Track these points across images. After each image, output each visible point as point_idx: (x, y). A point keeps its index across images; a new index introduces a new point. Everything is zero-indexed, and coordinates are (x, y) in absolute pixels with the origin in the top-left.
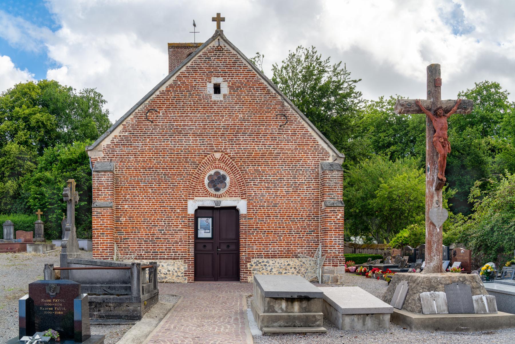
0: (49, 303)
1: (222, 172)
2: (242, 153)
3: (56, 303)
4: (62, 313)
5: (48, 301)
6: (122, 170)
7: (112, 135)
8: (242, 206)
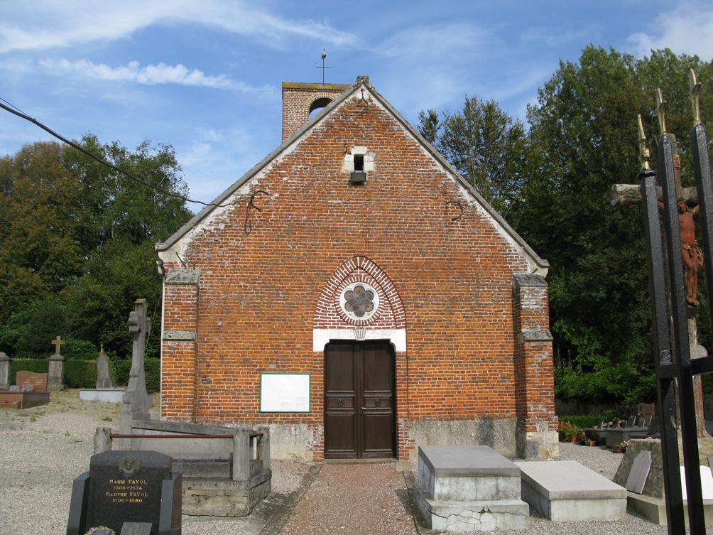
0: (122, 485)
1: (367, 287)
2: (397, 259)
3: (133, 485)
4: (141, 501)
5: (119, 482)
6: (212, 283)
7: (198, 229)
8: (399, 339)
